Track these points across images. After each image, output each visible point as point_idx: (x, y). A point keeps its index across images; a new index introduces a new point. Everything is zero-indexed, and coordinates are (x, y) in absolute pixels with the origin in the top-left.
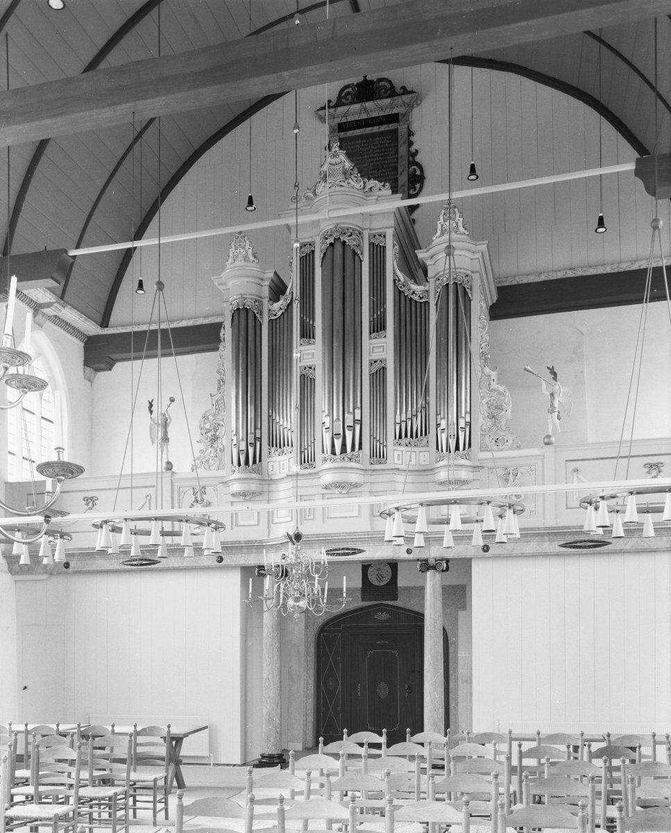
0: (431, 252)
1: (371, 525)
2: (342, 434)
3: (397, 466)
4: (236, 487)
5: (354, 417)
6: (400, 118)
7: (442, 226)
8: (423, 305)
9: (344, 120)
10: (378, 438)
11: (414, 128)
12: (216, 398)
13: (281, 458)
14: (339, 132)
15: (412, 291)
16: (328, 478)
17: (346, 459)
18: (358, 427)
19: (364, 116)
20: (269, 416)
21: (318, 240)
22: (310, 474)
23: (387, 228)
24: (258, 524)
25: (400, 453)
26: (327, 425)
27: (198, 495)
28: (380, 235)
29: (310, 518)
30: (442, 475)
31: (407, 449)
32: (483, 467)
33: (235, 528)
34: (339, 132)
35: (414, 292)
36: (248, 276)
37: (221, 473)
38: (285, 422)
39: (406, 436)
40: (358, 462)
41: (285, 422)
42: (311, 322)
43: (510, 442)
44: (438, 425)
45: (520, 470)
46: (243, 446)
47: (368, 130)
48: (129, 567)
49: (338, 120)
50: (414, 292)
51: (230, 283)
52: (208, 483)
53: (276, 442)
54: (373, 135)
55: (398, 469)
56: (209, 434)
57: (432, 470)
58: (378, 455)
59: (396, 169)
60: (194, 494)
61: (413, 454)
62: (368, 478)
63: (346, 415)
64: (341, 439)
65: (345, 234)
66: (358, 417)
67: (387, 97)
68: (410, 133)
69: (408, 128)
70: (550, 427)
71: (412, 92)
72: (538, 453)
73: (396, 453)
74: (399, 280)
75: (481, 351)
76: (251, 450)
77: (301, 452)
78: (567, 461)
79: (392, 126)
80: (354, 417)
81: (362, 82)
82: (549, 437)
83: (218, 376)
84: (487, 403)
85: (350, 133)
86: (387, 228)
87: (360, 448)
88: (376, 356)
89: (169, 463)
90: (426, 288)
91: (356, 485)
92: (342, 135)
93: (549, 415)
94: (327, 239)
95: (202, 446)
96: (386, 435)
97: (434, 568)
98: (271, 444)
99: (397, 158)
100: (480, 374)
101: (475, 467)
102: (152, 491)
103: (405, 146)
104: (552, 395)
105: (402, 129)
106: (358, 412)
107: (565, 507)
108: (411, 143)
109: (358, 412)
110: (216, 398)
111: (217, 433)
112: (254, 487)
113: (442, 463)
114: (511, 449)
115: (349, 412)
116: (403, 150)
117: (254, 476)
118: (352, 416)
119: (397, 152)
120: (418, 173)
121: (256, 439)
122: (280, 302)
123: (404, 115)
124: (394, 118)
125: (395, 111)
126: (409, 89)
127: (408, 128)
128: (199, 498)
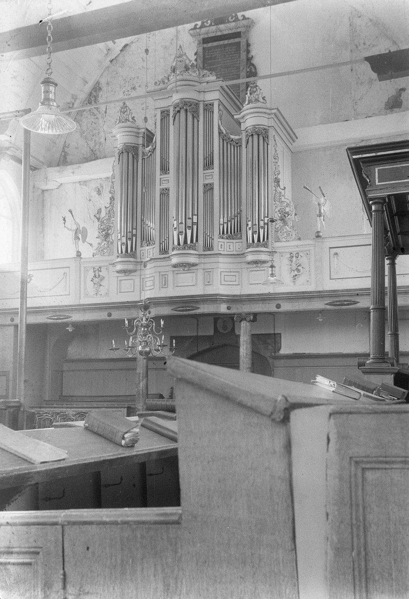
0: (242, 114)
1: (204, 290)
2: (184, 232)
3: (220, 252)
4: (119, 267)
5: (192, 221)
6: (242, 34)
7: (249, 97)
8: (239, 147)
9: (206, 36)
10: (208, 234)
11: (251, 42)
12: (108, 209)
13: (148, 248)
14: (203, 44)
15: (231, 140)
16: (175, 260)
17: (186, 248)
18: (195, 227)
19: (219, 34)
20: (142, 220)
21: (171, 109)
22: (164, 258)
23: (214, 100)
24: (221, 284)
25: (223, 244)
26: (175, 226)
27: (97, 272)
28: (210, 105)
29: (165, 286)
30: (250, 258)
31: (228, 241)
32: (276, 252)
33: (210, 283)
34: (203, 44)
35: (232, 140)
36: (124, 132)
37: (109, 258)
38: (151, 224)
39: (227, 232)
40: (195, 250)
41: (151, 224)
42: (167, 160)
43: (294, 236)
44: (247, 225)
45: (300, 254)
46: (124, 240)
47: (221, 43)
48: (190, 305)
49: (202, 37)
50: (232, 140)
51: (118, 135)
52: (103, 264)
53: (147, 240)
54: (225, 46)
55: (220, 254)
56: (104, 233)
57: (243, 254)
58: (208, 247)
59: (238, 68)
60: (94, 272)
61: (231, 244)
62: (203, 260)
63: (187, 220)
64: (183, 235)
65: (187, 104)
66: (195, 221)
67: (233, 21)
68: (248, 45)
69: (247, 41)
70: (319, 226)
71: (248, 18)
72: (312, 243)
73: (220, 244)
74: (222, 133)
75: (275, 177)
76: (129, 243)
77: (160, 243)
78: (330, 248)
79: (237, 40)
80: (192, 221)
81: (371, 64)
82: (318, 232)
83: (110, 195)
84: (279, 211)
85: (210, 45)
86: (214, 100)
87: (197, 240)
88: (207, 182)
89: (78, 252)
90: (240, 137)
91: (194, 265)
92: (205, 45)
93: (318, 218)
94: (176, 108)
95: (99, 241)
96: (142, 235)
97: (245, 319)
98: (142, 239)
99: (240, 61)
100: (274, 191)
101: (199, 255)
102: (66, 270)
103: (245, 53)
104: (319, 204)
105: (243, 41)
106: (195, 218)
107: (329, 278)
108: (248, 52)
109: (195, 218)
110: (108, 209)
111: (109, 232)
112: (131, 267)
113: (249, 250)
114: (294, 240)
115: (189, 218)
116: (243, 55)
117: (132, 259)
118: (191, 220)
119: (239, 57)
120: (254, 71)
121: (133, 235)
122: (149, 148)
123: (244, 33)
124: (237, 35)
125: (239, 30)
126: (247, 17)
127: (247, 41)
128: (97, 275)
